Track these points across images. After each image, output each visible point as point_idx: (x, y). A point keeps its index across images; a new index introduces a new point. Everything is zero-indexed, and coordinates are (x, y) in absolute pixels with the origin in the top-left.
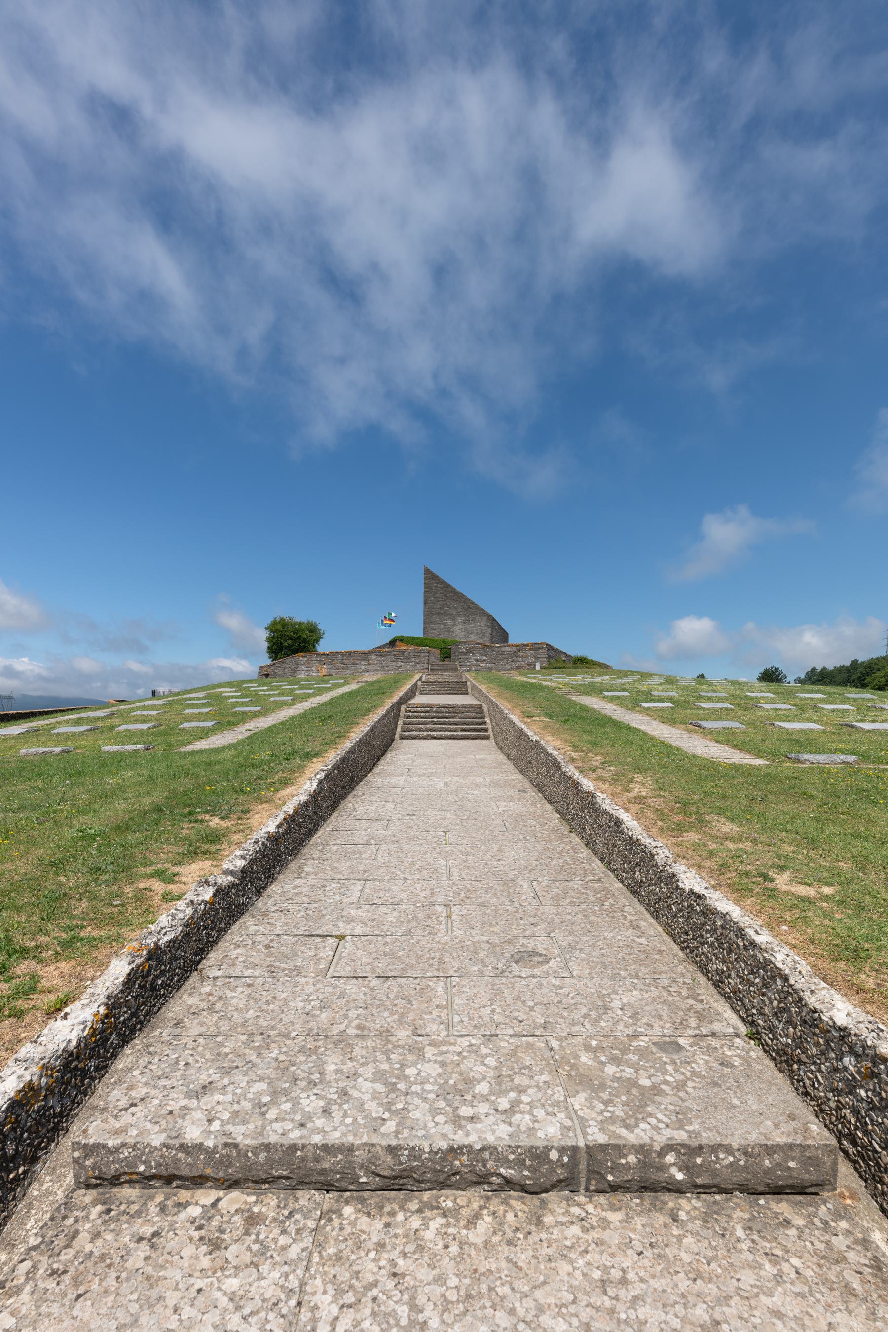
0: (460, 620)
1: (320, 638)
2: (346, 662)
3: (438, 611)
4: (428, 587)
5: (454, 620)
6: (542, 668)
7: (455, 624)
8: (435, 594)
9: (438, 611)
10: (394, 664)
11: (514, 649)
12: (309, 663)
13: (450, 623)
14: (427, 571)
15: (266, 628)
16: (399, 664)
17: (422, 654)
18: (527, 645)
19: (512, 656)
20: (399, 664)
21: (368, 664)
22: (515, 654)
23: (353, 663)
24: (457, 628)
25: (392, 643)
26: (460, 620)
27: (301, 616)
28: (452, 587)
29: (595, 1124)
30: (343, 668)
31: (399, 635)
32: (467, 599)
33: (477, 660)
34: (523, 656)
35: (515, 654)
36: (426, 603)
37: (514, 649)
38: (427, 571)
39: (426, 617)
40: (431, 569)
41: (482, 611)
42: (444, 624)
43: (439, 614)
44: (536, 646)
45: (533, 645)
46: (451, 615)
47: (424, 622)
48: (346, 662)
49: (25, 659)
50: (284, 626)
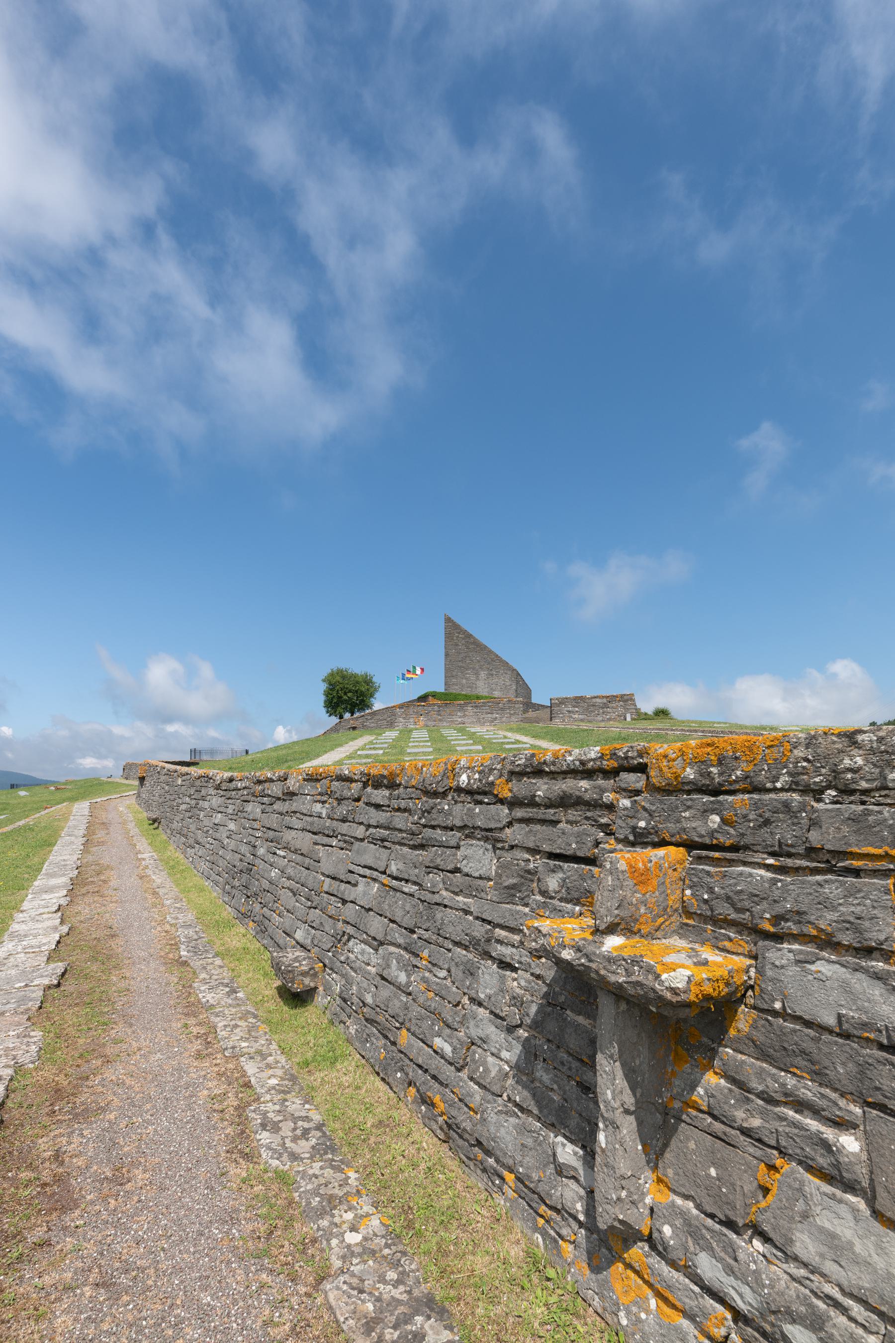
0: (483, 674)
1: (376, 690)
2: (442, 713)
3: (460, 664)
4: (449, 636)
5: (477, 674)
6: (632, 719)
7: (478, 679)
8: (457, 645)
9: (460, 664)
10: (489, 715)
11: (605, 700)
12: (407, 715)
13: (473, 678)
14: (448, 620)
15: (324, 681)
16: (495, 715)
17: (517, 706)
18: (617, 697)
19: (603, 708)
20: (495, 715)
21: (465, 716)
22: (605, 706)
23: (450, 715)
24: (480, 684)
25: (423, 698)
26: (483, 674)
27: (357, 667)
28: (474, 638)
29: (302, 1156)
30: (440, 720)
31: (432, 690)
32: (490, 652)
33: (569, 712)
34: (613, 708)
35: (605, 706)
36: (447, 655)
37: (605, 700)
38: (448, 620)
39: (447, 670)
40: (453, 618)
41: (505, 664)
42: (466, 679)
43: (461, 667)
44: (625, 697)
45: (622, 696)
46: (474, 669)
47: (446, 677)
48: (442, 713)
49: (844, 668)
50: (344, 677)
